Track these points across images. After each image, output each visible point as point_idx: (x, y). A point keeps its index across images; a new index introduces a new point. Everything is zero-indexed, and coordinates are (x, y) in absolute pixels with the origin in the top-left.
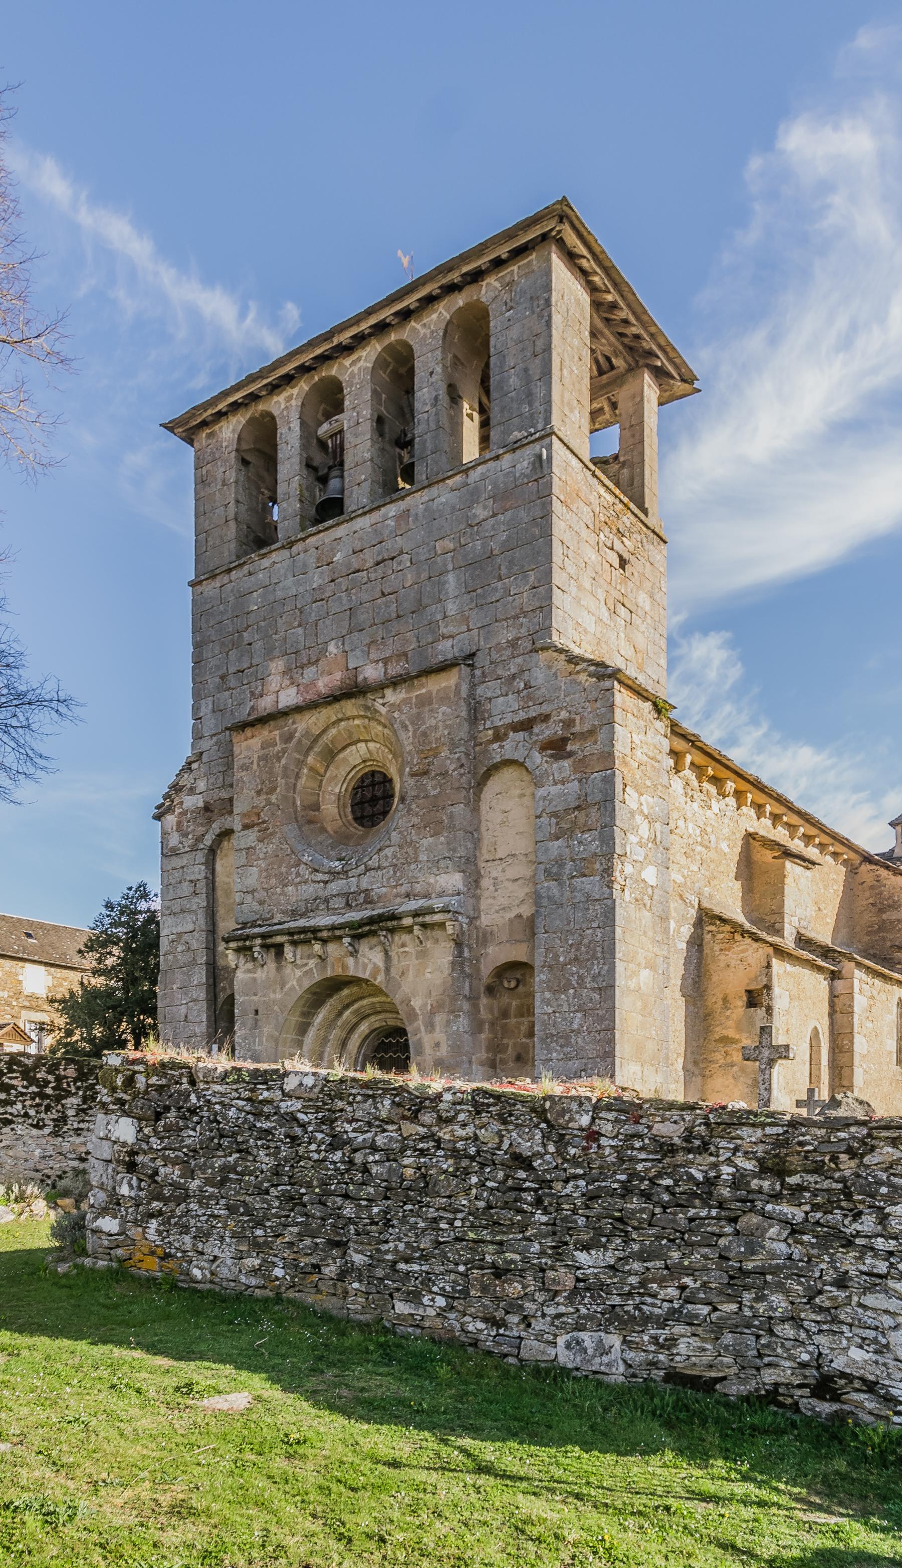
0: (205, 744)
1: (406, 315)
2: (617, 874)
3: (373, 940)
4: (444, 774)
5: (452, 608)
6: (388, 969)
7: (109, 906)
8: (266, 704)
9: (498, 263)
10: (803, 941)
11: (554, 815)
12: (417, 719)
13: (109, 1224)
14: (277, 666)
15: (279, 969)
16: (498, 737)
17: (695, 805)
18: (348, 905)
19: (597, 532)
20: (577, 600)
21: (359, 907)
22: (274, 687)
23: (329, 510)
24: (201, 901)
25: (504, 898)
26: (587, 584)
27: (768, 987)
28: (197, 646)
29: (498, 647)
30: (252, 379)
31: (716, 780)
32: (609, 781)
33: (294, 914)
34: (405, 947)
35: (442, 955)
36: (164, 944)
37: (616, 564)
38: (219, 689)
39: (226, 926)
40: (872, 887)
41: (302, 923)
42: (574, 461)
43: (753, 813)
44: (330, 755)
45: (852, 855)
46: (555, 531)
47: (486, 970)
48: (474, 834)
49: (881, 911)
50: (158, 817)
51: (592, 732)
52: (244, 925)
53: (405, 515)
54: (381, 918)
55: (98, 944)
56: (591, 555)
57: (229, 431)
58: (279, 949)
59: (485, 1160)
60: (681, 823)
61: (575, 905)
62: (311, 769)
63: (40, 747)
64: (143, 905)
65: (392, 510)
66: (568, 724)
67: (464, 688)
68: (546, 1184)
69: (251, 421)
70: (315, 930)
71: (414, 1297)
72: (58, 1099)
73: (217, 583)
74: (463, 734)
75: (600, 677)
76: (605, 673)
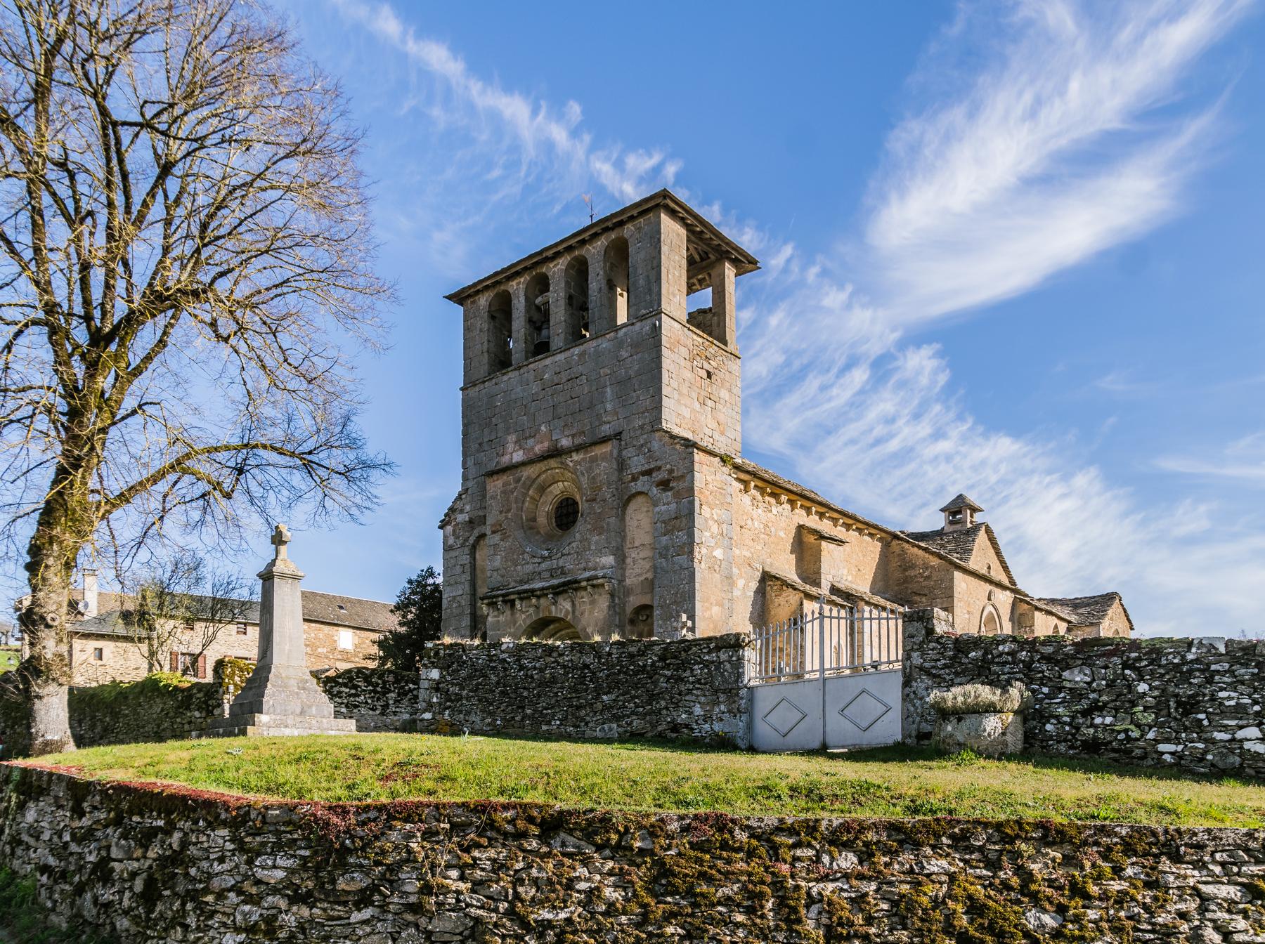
0: (470, 484)
2: (696, 554)
3: (566, 596)
4: (604, 501)
5: (609, 406)
6: (574, 612)
7: (410, 582)
8: (505, 460)
9: (632, 218)
10: (834, 590)
11: (664, 522)
13: (428, 716)
14: (512, 438)
15: (512, 614)
16: (634, 479)
18: (552, 576)
19: (692, 360)
20: (679, 401)
21: (558, 577)
22: (510, 450)
23: (541, 348)
24: (467, 577)
25: (638, 569)
26: (685, 391)
28: (464, 425)
29: (634, 429)
30: (496, 274)
31: (773, 495)
32: (692, 503)
33: (521, 582)
34: (584, 598)
35: (603, 603)
36: (445, 603)
37: (705, 376)
38: (478, 451)
39: (482, 590)
40: (899, 555)
41: (526, 587)
42: (676, 324)
43: (804, 512)
44: (542, 489)
45: (884, 535)
46: (664, 365)
47: (629, 610)
48: (622, 533)
49: (905, 570)
50: (441, 527)
51: (683, 476)
52: (493, 590)
53: (582, 355)
54: (570, 582)
55: (401, 607)
56: (688, 374)
57: (483, 300)
58: (512, 603)
59: (574, 668)
60: (749, 522)
61: (675, 572)
62: (532, 498)
63: (375, 492)
64: (431, 581)
65: (576, 350)
67: (615, 453)
68: (594, 673)
69: (497, 295)
70: (533, 591)
71: (549, 723)
72: (384, 694)
73: (477, 389)
74: (614, 478)
75: (687, 447)
76: (690, 445)
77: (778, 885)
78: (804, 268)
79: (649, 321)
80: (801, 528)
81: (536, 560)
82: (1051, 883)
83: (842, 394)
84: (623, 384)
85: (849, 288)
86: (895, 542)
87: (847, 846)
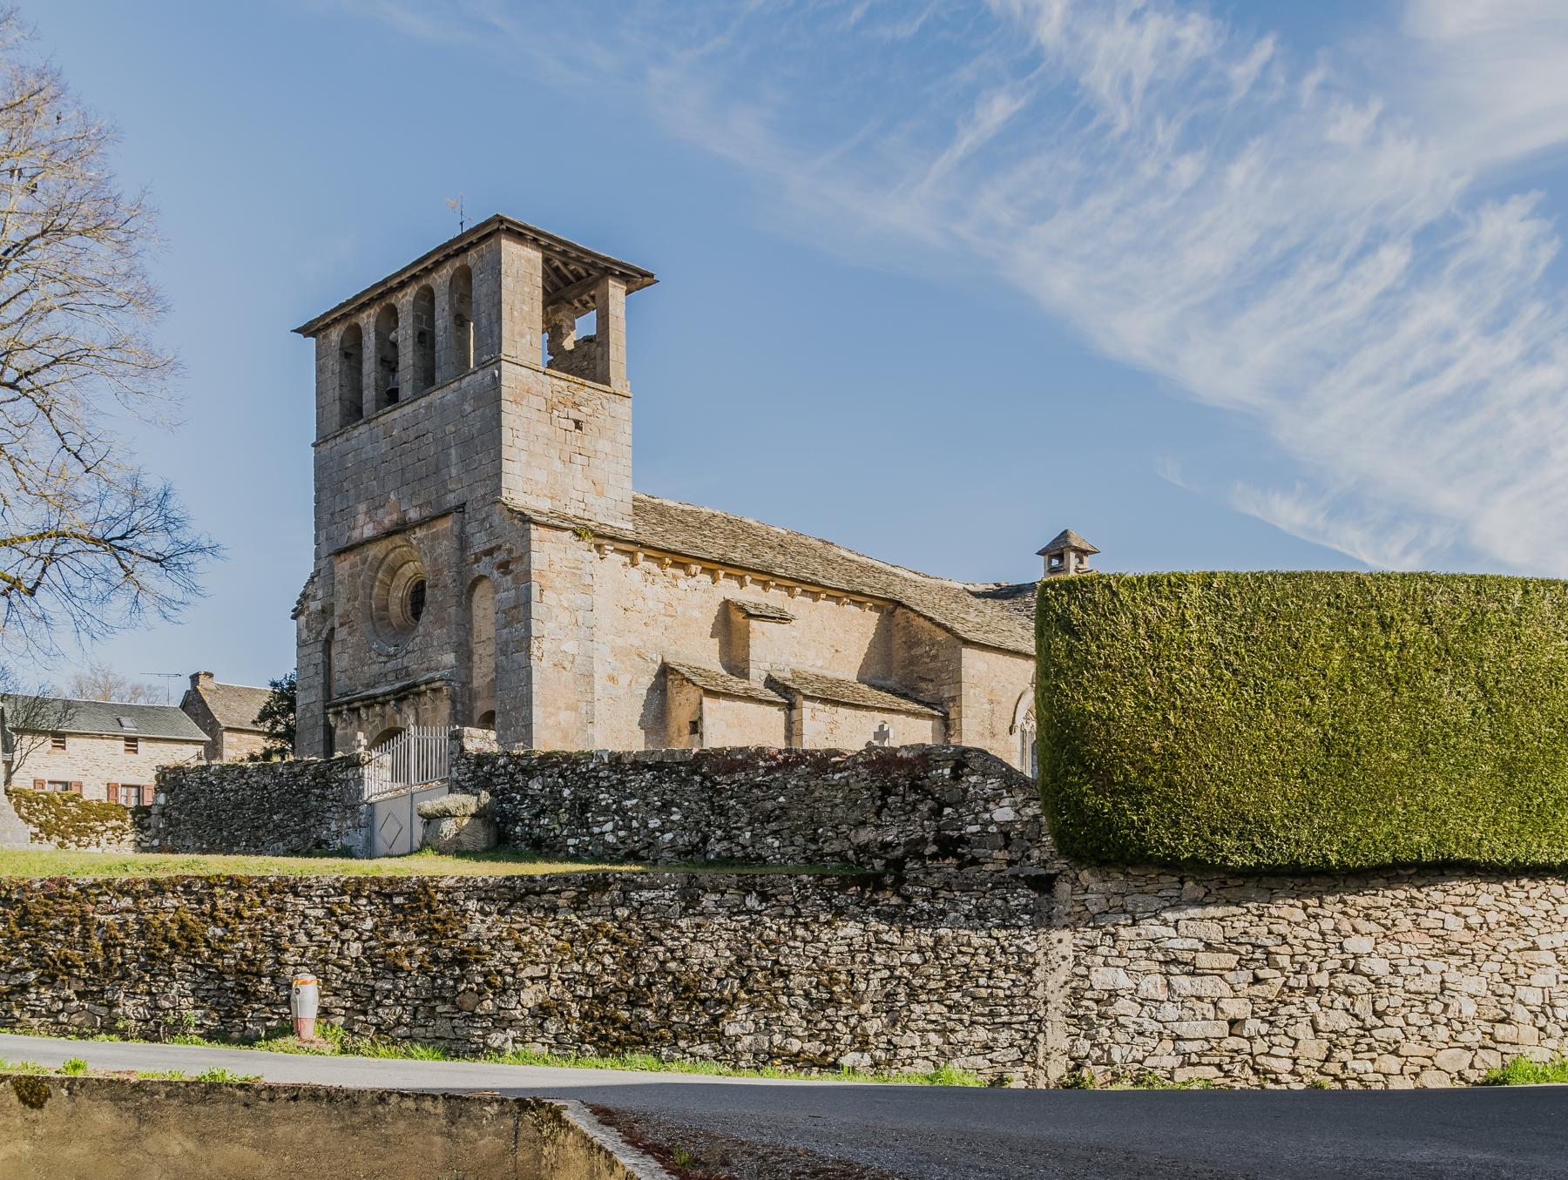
1: (428, 271)
2: (534, 649)
4: (445, 587)
5: (454, 472)
9: (472, 245)
10: (771, 683)
16: (477, 560)
17: (657, 587)
22: (360, 523)
23: (391, 397)
24: (320, 679)
27: (701, 718)
28: (317, 490)
30: (342, 306)
31: (675, 564)
33: (368, 686)
41: (371, 692)
44: (393, 571)
49: (910, 648)
50: (294, 618)
51: (521, 558)
53: (429, 406)
57: (335, 334)
66: (510, 551)
70: (375, 697)
77: (83, 918)
79: (489, 370)
80: (726, 603)
81: (383, 659)
82: (227, 911)
83: (1360, 293)
84: (466, 443)
85: (1376, 106)
86: (899, 611)
87: (127, 893)
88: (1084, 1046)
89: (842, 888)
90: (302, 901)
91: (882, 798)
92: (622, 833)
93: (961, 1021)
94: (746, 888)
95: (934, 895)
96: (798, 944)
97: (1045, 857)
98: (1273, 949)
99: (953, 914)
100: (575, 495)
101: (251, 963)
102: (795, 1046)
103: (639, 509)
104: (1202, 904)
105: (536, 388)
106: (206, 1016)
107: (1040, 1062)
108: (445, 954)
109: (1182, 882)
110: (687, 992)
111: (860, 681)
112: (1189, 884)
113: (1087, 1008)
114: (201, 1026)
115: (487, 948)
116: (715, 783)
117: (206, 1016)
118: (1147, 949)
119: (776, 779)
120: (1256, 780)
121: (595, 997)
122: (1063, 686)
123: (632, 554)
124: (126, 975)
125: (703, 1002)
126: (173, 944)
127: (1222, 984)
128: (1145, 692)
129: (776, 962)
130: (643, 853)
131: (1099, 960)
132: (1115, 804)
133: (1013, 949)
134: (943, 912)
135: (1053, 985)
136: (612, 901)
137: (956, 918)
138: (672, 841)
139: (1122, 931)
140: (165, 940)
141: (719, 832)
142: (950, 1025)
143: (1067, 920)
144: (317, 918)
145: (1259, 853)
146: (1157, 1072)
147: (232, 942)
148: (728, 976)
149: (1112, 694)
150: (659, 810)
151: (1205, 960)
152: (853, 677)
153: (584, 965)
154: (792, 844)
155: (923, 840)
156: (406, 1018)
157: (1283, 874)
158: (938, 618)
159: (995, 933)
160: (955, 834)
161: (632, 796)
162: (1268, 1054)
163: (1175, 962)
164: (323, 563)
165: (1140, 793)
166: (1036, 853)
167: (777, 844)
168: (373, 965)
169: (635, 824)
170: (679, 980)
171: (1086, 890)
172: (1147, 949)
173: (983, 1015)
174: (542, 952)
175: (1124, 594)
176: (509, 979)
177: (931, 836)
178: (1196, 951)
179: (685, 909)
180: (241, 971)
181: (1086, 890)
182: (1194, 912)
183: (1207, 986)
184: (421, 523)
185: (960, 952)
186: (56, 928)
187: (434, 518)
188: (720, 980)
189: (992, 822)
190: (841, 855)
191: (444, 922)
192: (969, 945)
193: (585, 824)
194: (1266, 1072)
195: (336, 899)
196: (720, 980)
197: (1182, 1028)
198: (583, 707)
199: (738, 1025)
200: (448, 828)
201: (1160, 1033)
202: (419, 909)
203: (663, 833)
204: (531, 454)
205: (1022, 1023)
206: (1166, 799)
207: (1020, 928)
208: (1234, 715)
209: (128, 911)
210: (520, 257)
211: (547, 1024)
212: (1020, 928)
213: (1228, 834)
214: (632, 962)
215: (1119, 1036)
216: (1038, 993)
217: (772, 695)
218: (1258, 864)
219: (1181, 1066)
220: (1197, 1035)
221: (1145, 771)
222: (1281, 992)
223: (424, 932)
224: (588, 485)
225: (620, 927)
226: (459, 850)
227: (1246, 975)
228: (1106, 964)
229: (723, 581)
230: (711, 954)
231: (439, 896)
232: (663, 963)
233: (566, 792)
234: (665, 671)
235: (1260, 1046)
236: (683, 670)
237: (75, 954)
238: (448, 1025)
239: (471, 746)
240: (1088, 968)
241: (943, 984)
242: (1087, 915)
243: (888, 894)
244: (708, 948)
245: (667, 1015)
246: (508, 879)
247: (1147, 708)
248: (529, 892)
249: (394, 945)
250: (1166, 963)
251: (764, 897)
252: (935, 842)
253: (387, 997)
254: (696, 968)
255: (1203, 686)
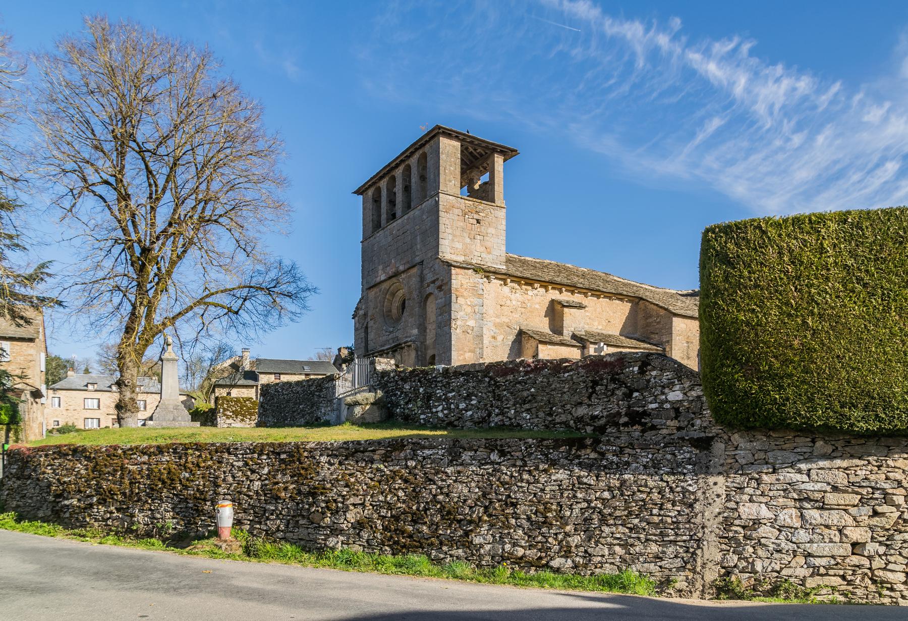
1: (408, 157)
2: (453, 325)
8: (378, 280)
9: (427, 142)
10: (574, 337)
12: (408, 283)
16: (428, 286)
23: (393, 217)
24: (363, 344)
30: (372, 179)
31: (526, 284)
33: (382, 346)
44: (393, 295)
57: (370, 192)
60: (509, 302)
66: (442, 280)
70: (383, 351)
77: (122, 468)
78: (849, 98)
86: (641, 302)
87: (144, 454)
88: (733, 559)
89: (556, 447)
90: (233, 457)
91: (592, 387)
92: (446, 412)
93: (639, 539)
94: (491, 448)
95: (622, 451)
96: (524, 484)
97: (705, 424)
98: (890, 491)
99: (634, 465)
100: (476, 253)
101: (202, 493)
102: (520, 552)
103: (509, 261)
104: (830, 457)
105: (457, 205)
106: (178, 523)
107: (698, 569)
108: (305, 489)
109: (813, 441)
110: (448, 515)
111: (621, 335)
112: (820, 443)
113: (736, 532)
114: (175, 529)
115: (328, 486)
116: (496, 382)
117: (178, 523)
118: (784, 490)
119: (530, 378)
120: (881, 366)
121: (392, 516)
122: (721, 302)
123: (504, 280)
124: (139, 500)
125: (459, 521)
126: (164, 482)
127: (846, 517)
128: (788, 304)
129: (509, 496)
130: (456, 423)
131: (746, 497)
132: (760, 387)
133: (679, 489)
134: (628, 464)
135: (709, 516)
136: (406, 456)
137: (637, 468)
138: (471, 416)
139: (765, 477)
140: (159, 480)
141: (497, 411)
142: (630, 541)
143: (721, 469)
144: (239, 467)
145: (881, 420)
146: (792, 580)
147: (192, 481)
148: (476, 505)
149: (760, 307)
150: (465, 398)
151: (832, 498)
152: (617, 333)
153: (386, 497)
154: (537, 416)
155: (619, 414)
156: (282, 527)
157: (899, 436)
158: (661, 304)
159: (665, 477)
160: (641, 409)
161: (453, 390)
162: (885, 569)
163: (808, 499)
164: (365, 294)
165: (782, 378)
166: (698, 422)
167: (528, 417)
168: (265, 495)
169: (452, 406)
170: (444, 507)
171: (736, 448)
172: (784, 490)
173: (655, 535)
174: (362, 488)
175: (772, 232)
176: (340, 505)
177: (623, 411)
178: (825, 492)
179: (451, 461)
180: (195, 498)
181: (736, 448)
182: (822, 464)
183: (834, 518)
184: (403, 272)
185: (639, 491)
186: (109, 473)
187: (409, 269)
188: (471, 507)
189: (667, 401)
190: (566, 424)
191: (306, 470)
192: (646, 486)
193: (429, 407)
194: (882, 582)
195: (250, 456)
196: (471, 507)
197: (814, 548)
198: (478, 351)
199: (482, 537)
200: (358, 411)
201: (794, 551)
202: (294, 462)
203: (467, 411)
204: (454, 236)
205: (684, 541)
206: (804, 382)
207: (684, 474)
208: (863, 318)
209: (144, 463)
210: (450, 145)
211: (362, 533)
212: (684, 474)
213: (856, 407)
214: (415, 495)
215: (760, 552)
216: (698, 520)
217: (574, 342)
218: (880, 429)
219: (812, 575)
220: (825, 553)
221: (786, 362)
222: (896, 523)
223: (295, 476)
224: (483, 249)
225: (410, 473)
226: (363, 423)
227: (867, 510)
228: (751, 501)
229: (551, 291)
230: (466, 491)
231: (306, 454)
232: (435, 496)
233: (421, 390)
234: (521, 333)
235: (878, 563)
236: (529, 332)
237: (115, 487)
238: (306, 532)
239: (379, 368)
240: (737, 503)
241: (626, 513)
242: (736, 466)
243: (588, 451)
244: (463, 485)
245: (436, 529)
246: (345, 443)
247: (789, 315)
248: (357, 451)
249: (277, 483)
250: (800, 500)
251: (502, 453)
252: (626, 415)
253: (272, 514)
254: (456, 500)
255: (838, 297)
